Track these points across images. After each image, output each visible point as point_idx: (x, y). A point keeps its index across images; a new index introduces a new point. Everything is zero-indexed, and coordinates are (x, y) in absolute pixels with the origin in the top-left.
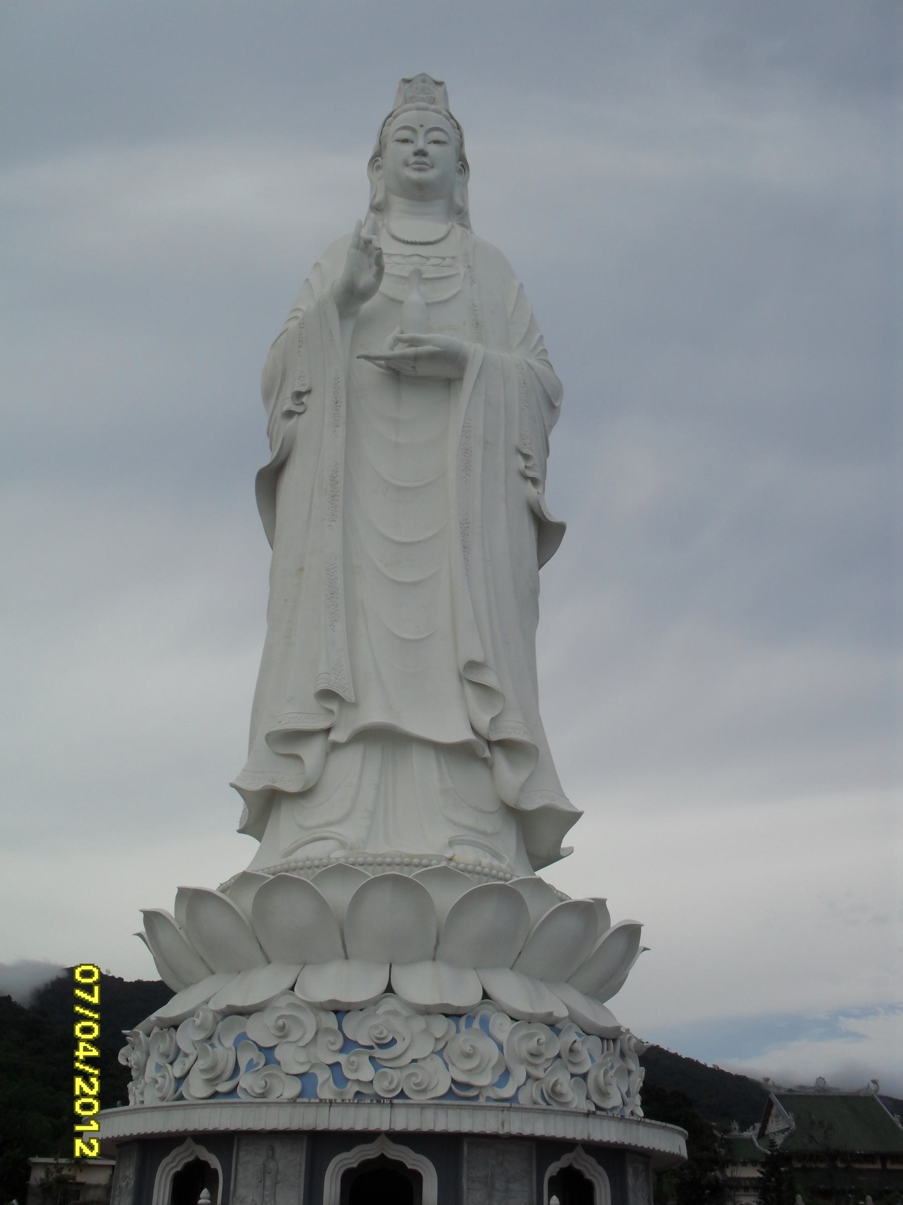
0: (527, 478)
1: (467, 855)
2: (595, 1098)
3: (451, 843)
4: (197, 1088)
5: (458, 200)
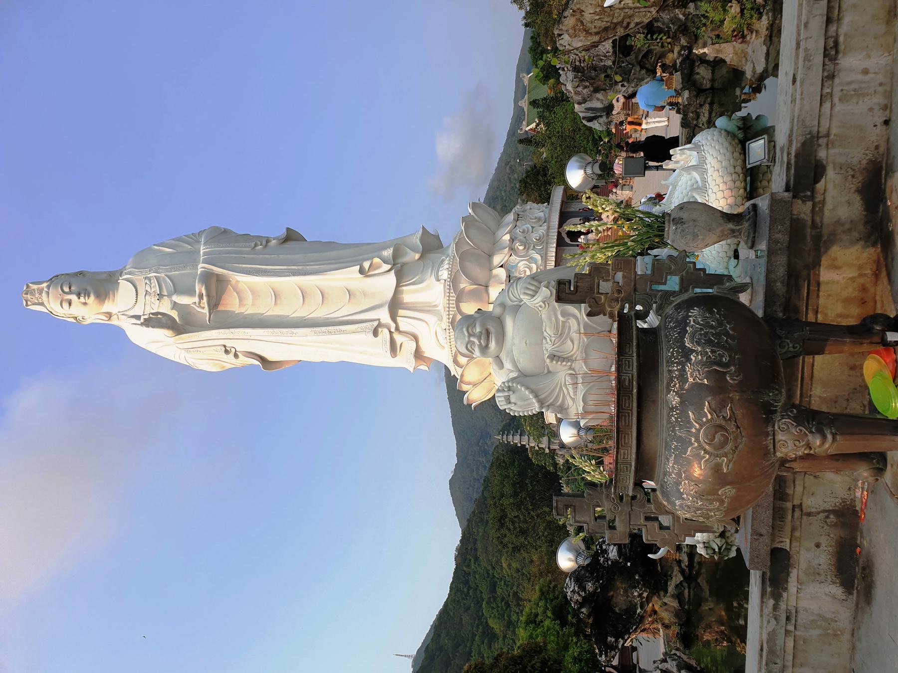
1: (444, 274)
2: (541, 223)
5: (104, 276)
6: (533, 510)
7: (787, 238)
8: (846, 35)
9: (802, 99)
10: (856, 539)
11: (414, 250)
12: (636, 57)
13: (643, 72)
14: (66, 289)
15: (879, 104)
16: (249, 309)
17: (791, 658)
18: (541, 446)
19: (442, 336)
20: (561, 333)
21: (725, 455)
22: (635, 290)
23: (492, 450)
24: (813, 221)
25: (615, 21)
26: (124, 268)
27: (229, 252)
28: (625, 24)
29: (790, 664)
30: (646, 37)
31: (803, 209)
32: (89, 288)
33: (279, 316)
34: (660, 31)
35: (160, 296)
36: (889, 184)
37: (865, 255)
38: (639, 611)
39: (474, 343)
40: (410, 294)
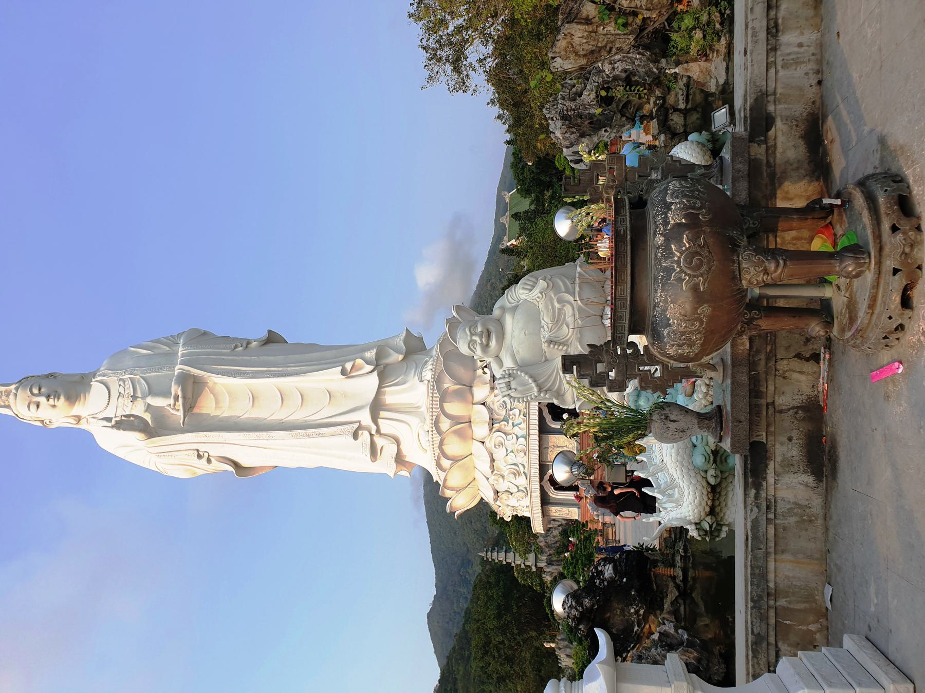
1: (428, 375)
6: (519, 634)
7: (746, 168)
8: (783, 18)
9: (752, 65)
10: (822, 431)
11: (398, 351)
12: (617, 106)
13: (624, 119)
14: (36, 391)
15: (812, 69)
16: (225, 411)
17: (772, 544)
18: (527, 563)
19: (424, 438)
20: (558, 319)
21: (701, 275)
22: (626, 180)
23: (473, 579)
24: (768, 161)
25: (600, 45)
26: (98, 370)
27: (208, 354)
28: (608, 48)
29: (772, 550)
30: (625, 89)
31: (758, 151)
32: (59, 390)
33: (255, 419)
34: (637, 83)
35: (134, 398)
36: (825, 128)
37: (811, 188)
38: (636, 628)
39: (475, 342)
40: (392, 396)
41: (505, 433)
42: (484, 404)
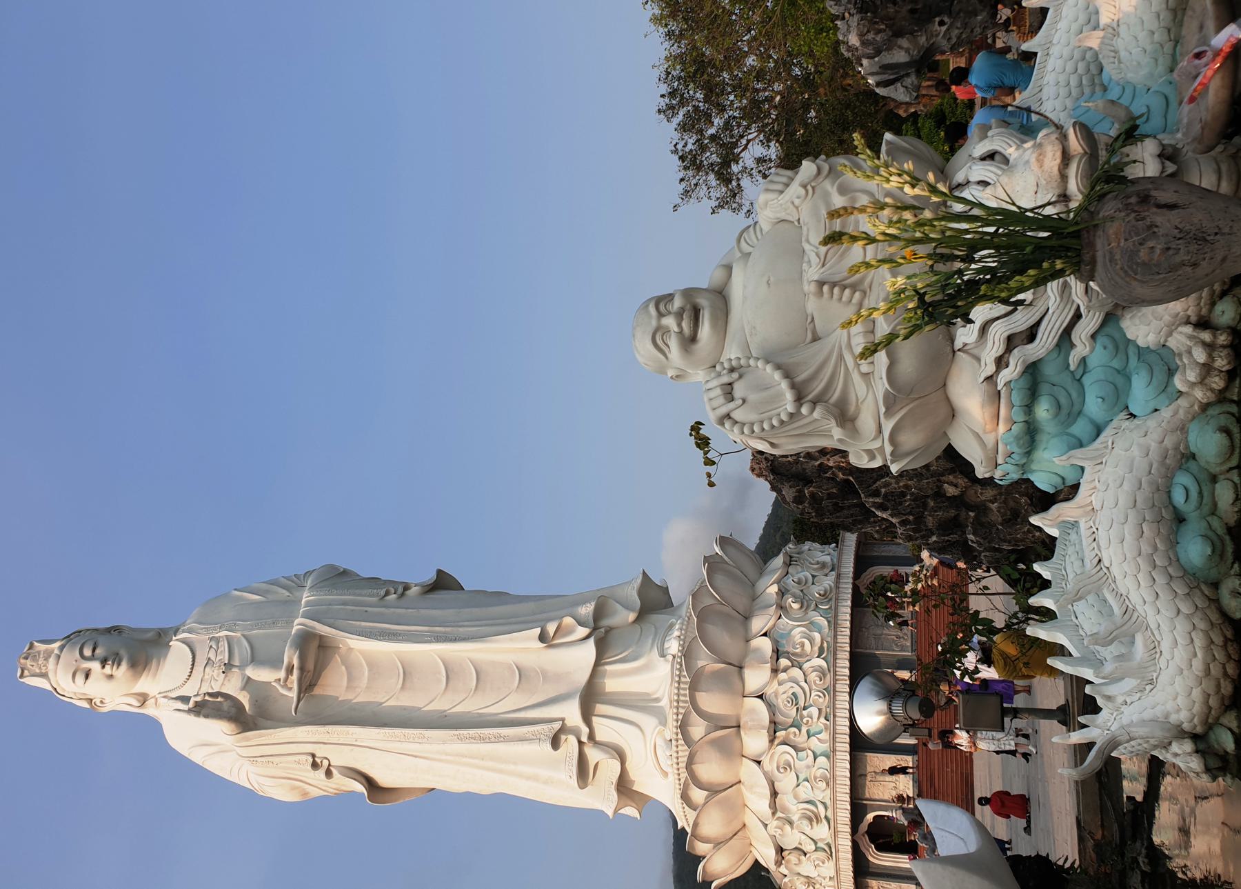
0: (403, 595)
1: (673, 646)
2: (826, 571)
3: (663, 655)
4: (822, 832)
5: (149, 635)
11: (628, 607)
14: (88, 652)
27: (345, 603)
33: (405, 708)
40: (616, 681)
41: (794, 747)
42: (761, 697)
